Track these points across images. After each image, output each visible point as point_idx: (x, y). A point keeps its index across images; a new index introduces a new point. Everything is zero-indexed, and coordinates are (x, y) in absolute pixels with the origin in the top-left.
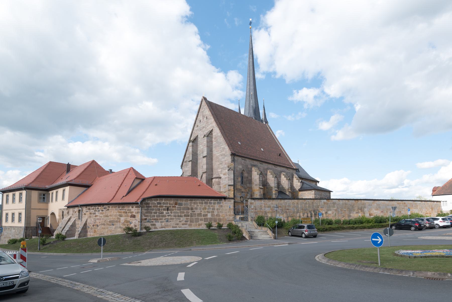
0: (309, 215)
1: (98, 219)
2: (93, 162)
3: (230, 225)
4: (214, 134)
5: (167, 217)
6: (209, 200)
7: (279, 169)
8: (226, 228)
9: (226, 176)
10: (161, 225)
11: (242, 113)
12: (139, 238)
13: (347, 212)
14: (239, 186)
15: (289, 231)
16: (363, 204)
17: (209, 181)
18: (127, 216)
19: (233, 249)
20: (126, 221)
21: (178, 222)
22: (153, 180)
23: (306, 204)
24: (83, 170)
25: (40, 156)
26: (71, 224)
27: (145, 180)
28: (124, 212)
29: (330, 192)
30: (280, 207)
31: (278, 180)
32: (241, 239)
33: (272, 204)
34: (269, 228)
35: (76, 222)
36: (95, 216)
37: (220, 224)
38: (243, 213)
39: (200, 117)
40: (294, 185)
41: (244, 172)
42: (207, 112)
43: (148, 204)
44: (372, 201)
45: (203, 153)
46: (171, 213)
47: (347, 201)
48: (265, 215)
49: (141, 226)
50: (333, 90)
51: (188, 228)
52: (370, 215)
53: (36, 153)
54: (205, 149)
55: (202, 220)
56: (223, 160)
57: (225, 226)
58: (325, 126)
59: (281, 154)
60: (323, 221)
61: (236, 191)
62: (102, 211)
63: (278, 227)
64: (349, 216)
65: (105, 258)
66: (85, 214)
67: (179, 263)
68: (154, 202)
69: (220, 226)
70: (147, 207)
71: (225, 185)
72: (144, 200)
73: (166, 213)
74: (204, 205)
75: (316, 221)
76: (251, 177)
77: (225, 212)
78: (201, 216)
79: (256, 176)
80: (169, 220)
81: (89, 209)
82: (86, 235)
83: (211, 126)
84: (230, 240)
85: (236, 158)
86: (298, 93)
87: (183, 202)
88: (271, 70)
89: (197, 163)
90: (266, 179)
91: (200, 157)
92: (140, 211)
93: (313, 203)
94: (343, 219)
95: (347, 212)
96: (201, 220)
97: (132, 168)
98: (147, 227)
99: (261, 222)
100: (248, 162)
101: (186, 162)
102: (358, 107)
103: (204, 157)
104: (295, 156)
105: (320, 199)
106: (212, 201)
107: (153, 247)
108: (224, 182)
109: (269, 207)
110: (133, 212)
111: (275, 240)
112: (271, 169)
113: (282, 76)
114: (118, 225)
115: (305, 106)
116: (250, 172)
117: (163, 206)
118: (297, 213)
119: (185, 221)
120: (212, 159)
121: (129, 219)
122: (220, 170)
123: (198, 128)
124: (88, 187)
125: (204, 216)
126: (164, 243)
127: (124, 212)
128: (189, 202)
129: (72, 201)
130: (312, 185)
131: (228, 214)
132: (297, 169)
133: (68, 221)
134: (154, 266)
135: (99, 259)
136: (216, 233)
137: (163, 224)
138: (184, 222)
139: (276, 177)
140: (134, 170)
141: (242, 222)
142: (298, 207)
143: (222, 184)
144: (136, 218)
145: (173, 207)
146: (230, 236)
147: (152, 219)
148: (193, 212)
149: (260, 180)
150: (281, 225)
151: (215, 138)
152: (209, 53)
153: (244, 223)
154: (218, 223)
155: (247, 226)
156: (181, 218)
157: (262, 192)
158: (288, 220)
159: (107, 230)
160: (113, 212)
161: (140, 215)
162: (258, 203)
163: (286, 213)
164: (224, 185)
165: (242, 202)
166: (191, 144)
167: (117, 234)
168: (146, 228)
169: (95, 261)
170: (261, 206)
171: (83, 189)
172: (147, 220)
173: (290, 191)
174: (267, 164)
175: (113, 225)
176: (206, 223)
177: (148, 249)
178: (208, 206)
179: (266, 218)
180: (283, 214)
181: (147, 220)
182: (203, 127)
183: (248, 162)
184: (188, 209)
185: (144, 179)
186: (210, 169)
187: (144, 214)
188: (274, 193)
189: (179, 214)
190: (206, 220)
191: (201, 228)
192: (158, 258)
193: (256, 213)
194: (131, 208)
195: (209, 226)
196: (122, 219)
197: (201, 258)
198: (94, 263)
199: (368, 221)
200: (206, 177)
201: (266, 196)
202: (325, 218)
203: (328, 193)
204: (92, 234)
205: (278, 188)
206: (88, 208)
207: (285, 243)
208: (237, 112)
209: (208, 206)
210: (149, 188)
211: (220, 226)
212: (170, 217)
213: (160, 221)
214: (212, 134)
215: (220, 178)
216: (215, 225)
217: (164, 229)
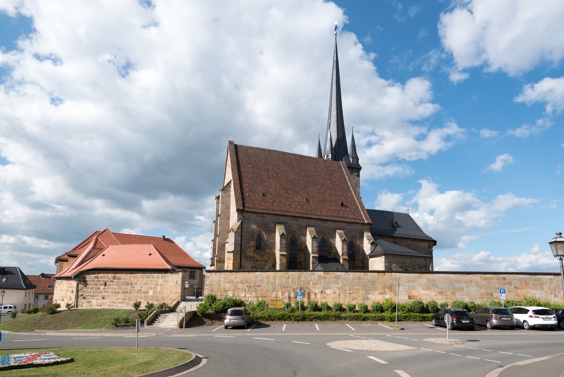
5: (104, 294)
21: (114, 300)
25: (199, 220)
30: (247, 282)
46: (108, 288)
52: (410, 297)
53: (197, 217)
61: (244, 260)
86: (533, 87)
88: (477, 63)
95: (362, 293)
113: (500, 69)
115: (549, 109)
118: (273, 291)
119: (123, 299)
131: (174, 291)
137: (99, 301)
145: (111, 281)
148: (132, 287)
152: (375, 62)
156: (119, 295)
178: (151, 281)
195: (137, 305)
209: (151, 281)
212: (107, 294)
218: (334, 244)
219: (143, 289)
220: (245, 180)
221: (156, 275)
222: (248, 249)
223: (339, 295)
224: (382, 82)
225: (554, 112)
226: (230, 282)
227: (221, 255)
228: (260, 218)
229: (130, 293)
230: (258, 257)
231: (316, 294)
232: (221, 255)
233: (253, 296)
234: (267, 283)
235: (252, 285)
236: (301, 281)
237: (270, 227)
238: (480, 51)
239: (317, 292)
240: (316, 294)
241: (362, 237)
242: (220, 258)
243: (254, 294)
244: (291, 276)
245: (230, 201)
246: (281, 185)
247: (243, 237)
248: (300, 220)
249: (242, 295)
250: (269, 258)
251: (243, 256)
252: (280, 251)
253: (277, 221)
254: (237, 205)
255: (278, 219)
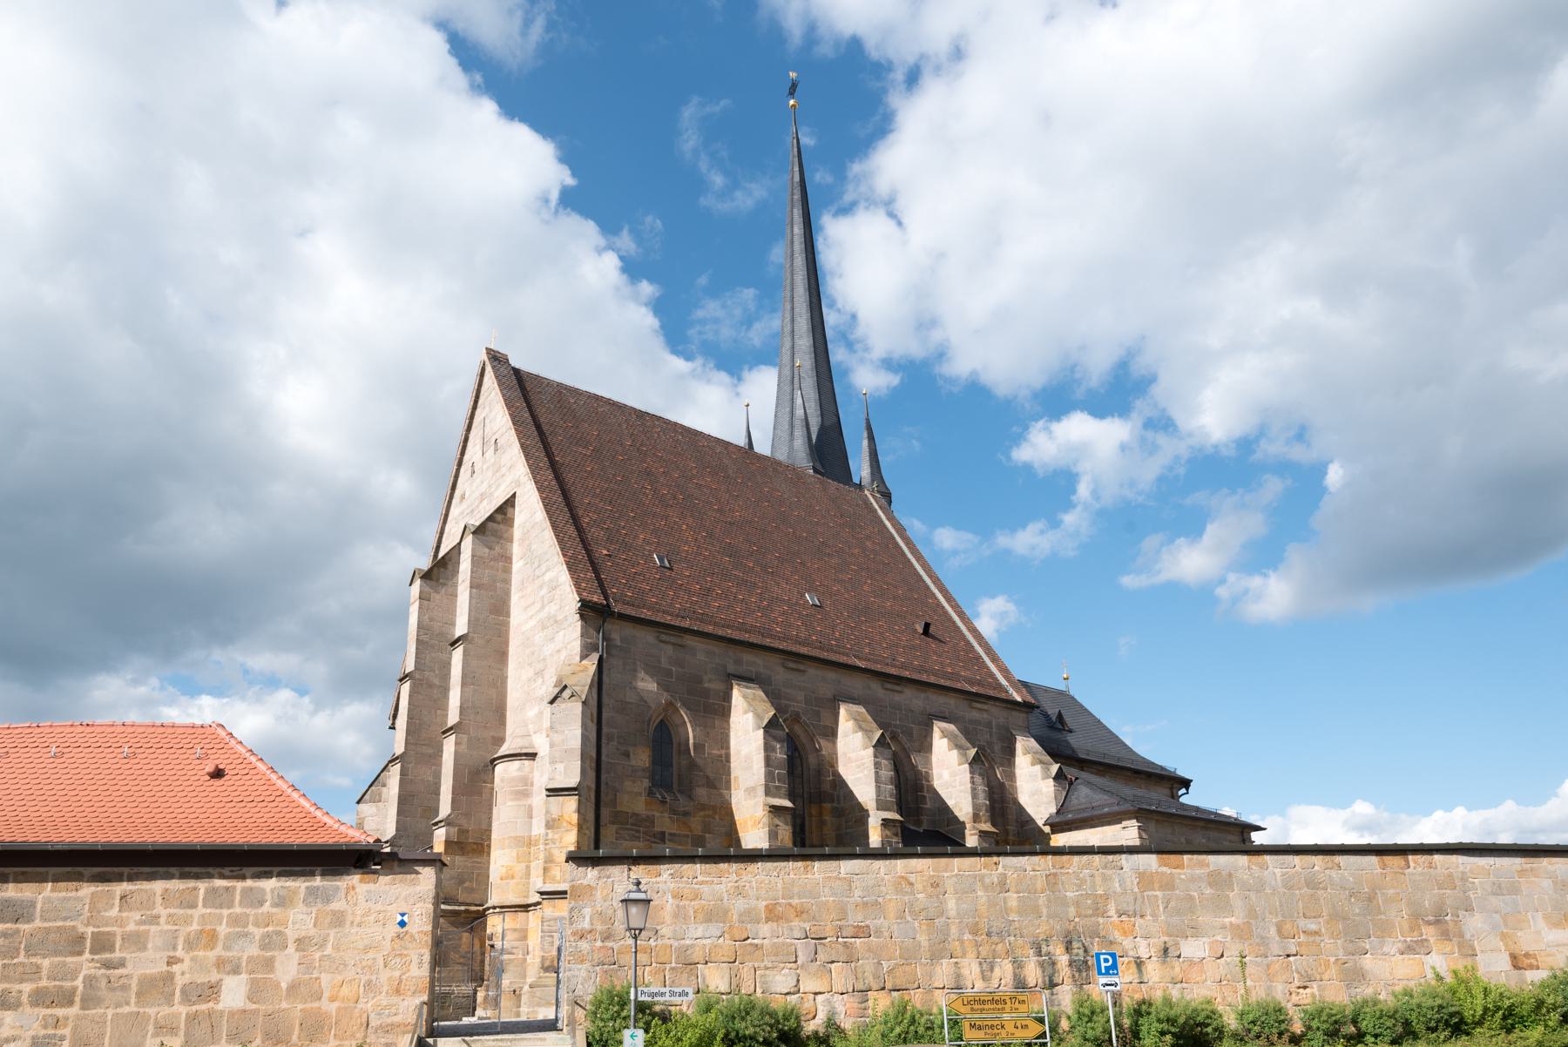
0: (1033, 974)
7: (914, 700)
13: (1327, 942)
16: (1450, 881)
23: (1003, 886)
30: (800, 913)
33: (739, 892)
42: (496, 416)
44: (1516, 862)
47: (1318, 861)
50: (1214, 413)
52: (1517, 962)
58: (1192, 562)
64: (1355, 976)
74: (201, 910)
88: (914, 348)
94: (1305, 997)
95: (1332, 947)
102: (1335, 475)
115: (1083, 490)
118: (935, 957)
131: (384, 976)
148: (108, 965)
149: (768, 762)
152: (658, 307)
178: (235, 920)
184: (75, 944)
199: (1509, 1013)
209: (235, 920)
214: (509, 522)
218: (928, 777)
219: (183, 974)
220: (582, 500)
221: (270, 885)
222: (627, 783)
223: (1243, 965)
224: (679, 364)
225: (1095, 494)
226: (710, 916)
227: (467, 815)
228: (669, 650)
229: (87, 1003)
230: (664, 822)
231: (1139, 964)
232: (467, 815)
233: (838, 987)
234: (901, 915)
235: (829, 930)
236: (1064, 903)
237: (706, 693)
238: (925, 323)
239: (1143, 953)
240: (1139, 964)
241: (1010, 752)
242: (462, 832)
243: (840, 976)
244: (1012, 877)
245: (507, 581)
246: (710, 535)
247: (605, 730)
248: (813, 672)
249: (781, 981)
250: (707, 828)
251: (605, 812)
252: (768, 793)
253: (731, 669)
254: (577, 585)
255: (738, 662)
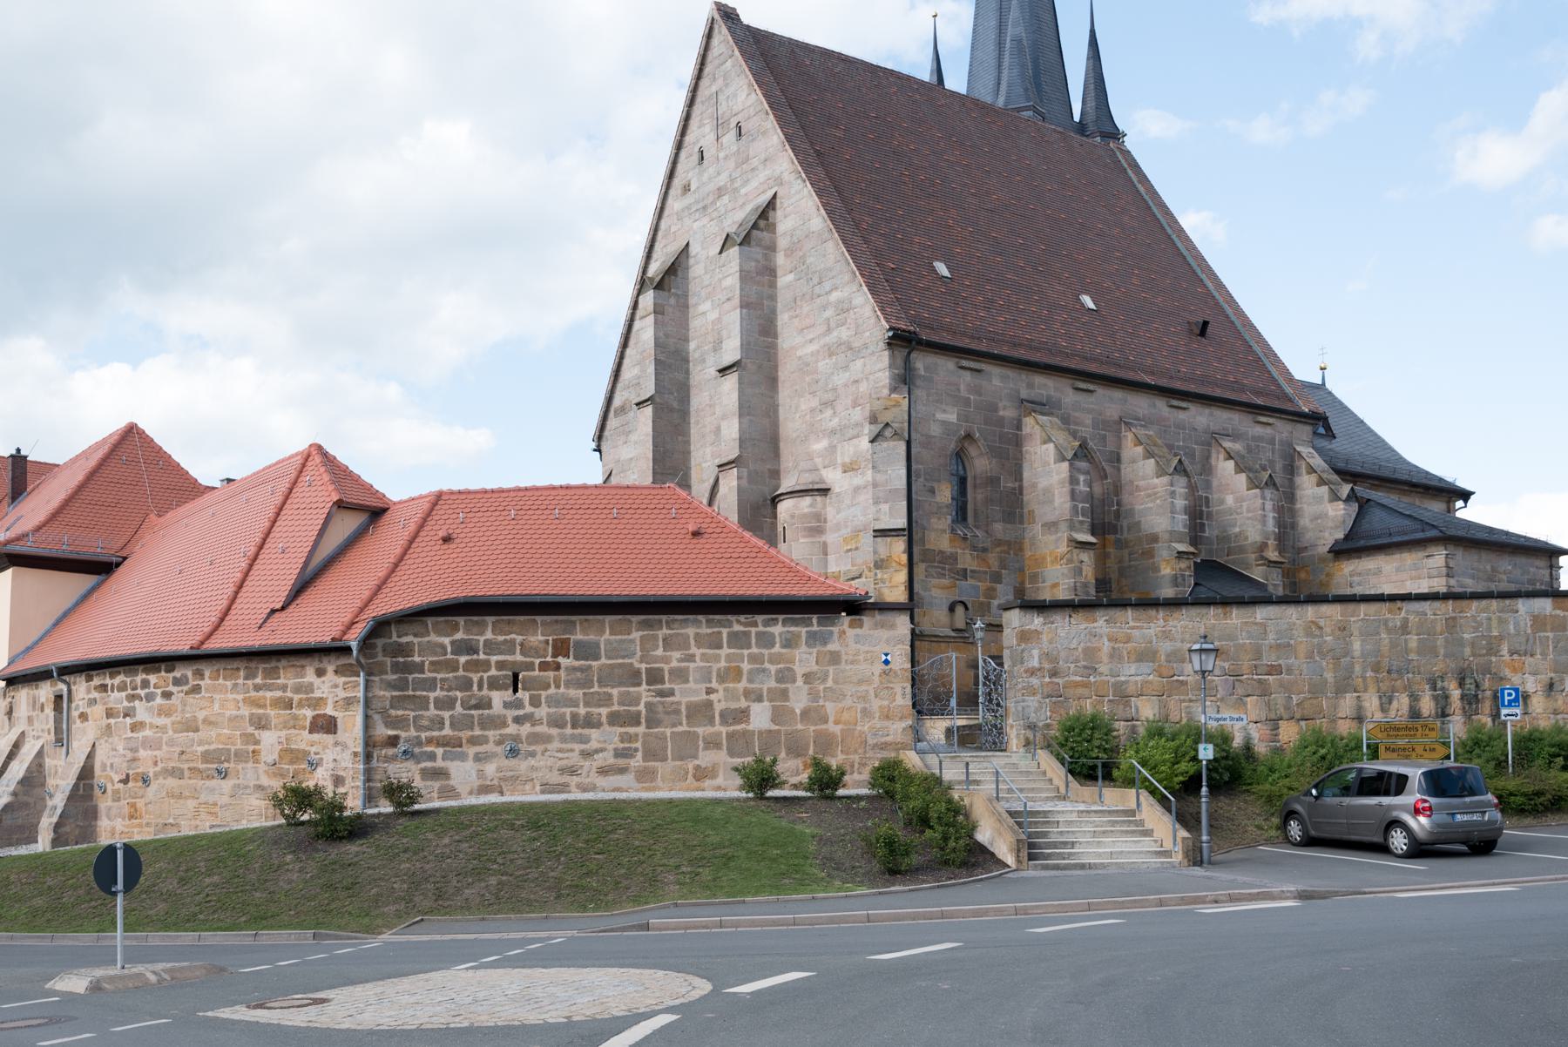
0: (1427, 705)
1: (148, 744)
2: (131, 433)
3: (889, 776)
4: (785, 223)
5: (512, 729)
6: (760, 618)
7: (1200, 418)
8: (865, 791)
9: (858, 480)
10: (481, 774)
11: (956, 81)
12: (352, 848)
14: (939, 535)
15: (1290, 815)
17: (760, 512)
18: (294, 723)
19: (917, 927)
20: (290, 754)
21: (574, 759)
22: (429, 514)
24: (80, 477)
26: (21, 775)
27: (387, 517)
28: (276, 703)
29: (1550, 554)
31: (1192, 488)
32: (964, 864)
33: (1166, 635)
34: (1153, 792)
35: (48, 762)
36: (134, 728)
37: (827, 769)
38: (969, 701)
39: (701, 133)
40: (1304, 521)
41: (972, 451)
42: (740, 93)
43: (405, 650)
45: (717, 346)
46: (535, 702)
48: (1120, 711)
49: (368, 780)
51: (633, 795)
54: (733, 319)
55: (718, 746)
56: (840, 379)
57: (858, 784)
59: (1212, 320)
60: (1528, 744)
61: (920, 569)
62: (167, 695)
63: (1210, 788)
65: (139, 969)
66: (83, 717)
67: (554, 1016)
68: (433, 638)
69: (826, 782)
70: (396, 668)
71: (856, 532)
72: (381, 627)
73: (507, 705)
74: (725, 651)
75: (1475, 745)
76: (1018, 474)
77: (855, 697)
78: (711, 722)
79: (1047, 472)
80: (524, 747)
81: (103, 688)
82: (88, 833)
83: (762, 176)
84: (893, 864)
85: (921, 362)
87: (604, 634)
89: (685, 414)
90: (1117, 489)
91: (703, 373)
92: (361, 694)
93: (1451, 623)
96: (712, 743)
97: (320, 448)
98: (400, 788)
99: (1090, 758)
100: (996, 382)
101: (622, 410)
103: (723, 371)
104: (1301, 335)
105: (1503, 595)
106: (777, 630)
107: (427, 904)
108: (848, 514)
109: (1145, 655)
110: (320, 701)
111: (1198, 871)
112: (1147, 422)
114: (250, 774)
116: (1010, 449)
117: (486, 665)
118: (1340, 690)
120: (772, 381)
121: (305, 740)
122: (820, 445)
123: (689, 199)
124: (102, 568)
125: (727, 717)
126: (493, 881)
127: (276, 703)
128: (636, 635)
129: (28, 649)
130: (1426, 516)
131: (876, 704)
132: (1317, 416)
133: (11, 756)
134: (391, 1034)
135: (99, 972)
136: (806, 825)
137: (490, 769)
138: (607, 758)
139: (1180, 469)
140: (328, 460)
141: (966, 755)
142: (1347, 652)
143: (838, 527)
144: (341, 735)
145: (544, 666)
146: (890, 844)
147: (430, 741)
148: (661, 694)
149: (1073, 495)
150: (1231, 773)
151: (790, 252)
153: (983, 765)
154: (816, 763)
155: (1001, 785)
156: (594, 734)
157: (1089, 573)
158: (1275, 737)
159: (191, 804)
160: (223, 700)
161: (359, 719)
162: (1067, 634)
163: (1264, 691)
164: (845, 532)
165: (963, 636)
166: (648, 299)
167: (244, 825)
168: (395, 792)
169: (75, 983)
170: (1090, 653)
171: (84, 581)
172: (402, 747)
173: (1273, 555)
174: (1118, 394)
175: (223, 774)
176: (738, 761)
177: (399, 916)
178: (753, 659)
179: (1121, 727)
180: (1240, 703)
181: (402, 747)
182: (720, 192)
183: (998, 381)
185: (385, 510)
186: (762, 445)
187: (383, 713)
188: (1168, 572)
189: (582, 711)
190: (737, 743)
191: (710, 794)
192: (437, 976)
193: (1056, 696)
194: (310, 676)
195: (761, 779)
196: (270, 741)
197: (705, 987)
198: (69, 997)
200: (740, 490)
201: (1113, 591)
202: (1544, 724)
203: (1542, 563)
204: (119, 824)
205: (1195, 540)
206: (97, 681)
207: (1269, 893)
208: (921, 83)
210: (408, 561)
211: (826, 782)
212: (526, 729)
213: (472, 751)
214: (772, 228)
215: (825, 492)
216: (794, 774)
217: (493, 798)
